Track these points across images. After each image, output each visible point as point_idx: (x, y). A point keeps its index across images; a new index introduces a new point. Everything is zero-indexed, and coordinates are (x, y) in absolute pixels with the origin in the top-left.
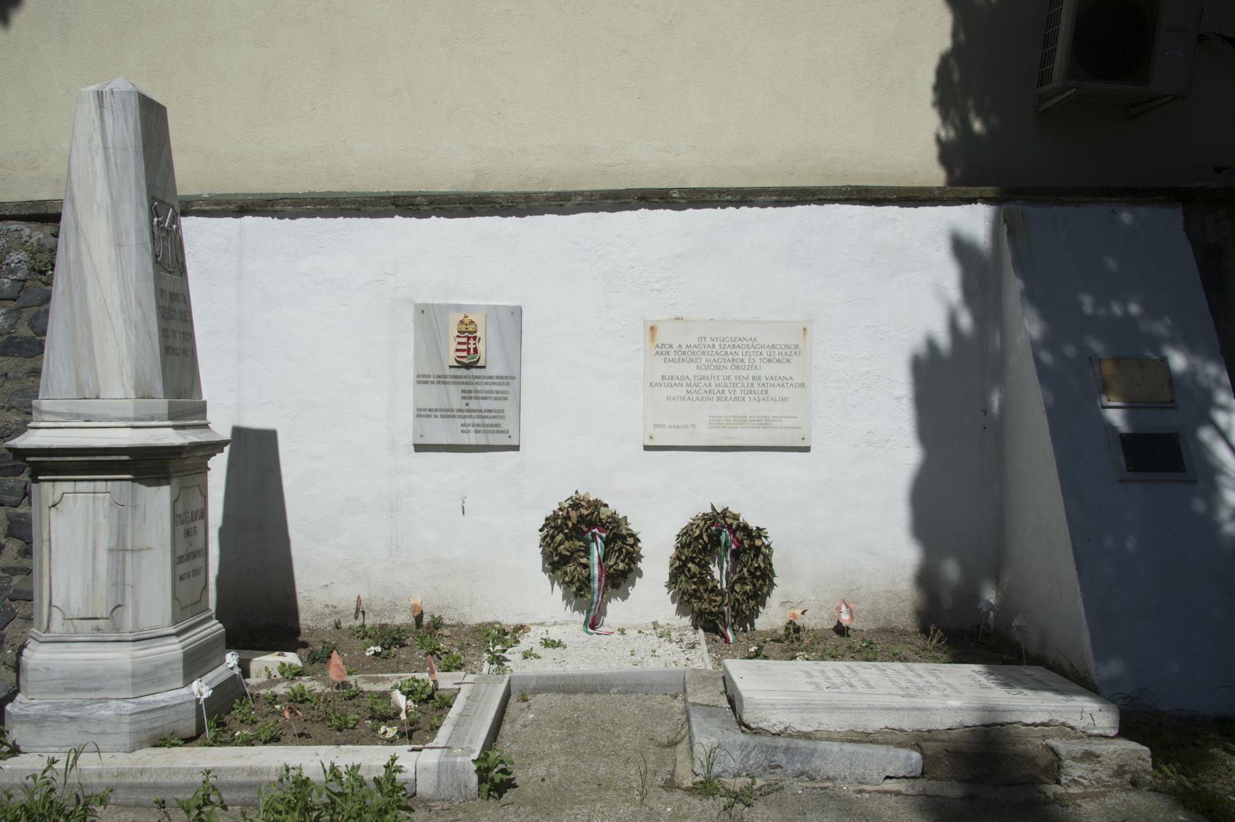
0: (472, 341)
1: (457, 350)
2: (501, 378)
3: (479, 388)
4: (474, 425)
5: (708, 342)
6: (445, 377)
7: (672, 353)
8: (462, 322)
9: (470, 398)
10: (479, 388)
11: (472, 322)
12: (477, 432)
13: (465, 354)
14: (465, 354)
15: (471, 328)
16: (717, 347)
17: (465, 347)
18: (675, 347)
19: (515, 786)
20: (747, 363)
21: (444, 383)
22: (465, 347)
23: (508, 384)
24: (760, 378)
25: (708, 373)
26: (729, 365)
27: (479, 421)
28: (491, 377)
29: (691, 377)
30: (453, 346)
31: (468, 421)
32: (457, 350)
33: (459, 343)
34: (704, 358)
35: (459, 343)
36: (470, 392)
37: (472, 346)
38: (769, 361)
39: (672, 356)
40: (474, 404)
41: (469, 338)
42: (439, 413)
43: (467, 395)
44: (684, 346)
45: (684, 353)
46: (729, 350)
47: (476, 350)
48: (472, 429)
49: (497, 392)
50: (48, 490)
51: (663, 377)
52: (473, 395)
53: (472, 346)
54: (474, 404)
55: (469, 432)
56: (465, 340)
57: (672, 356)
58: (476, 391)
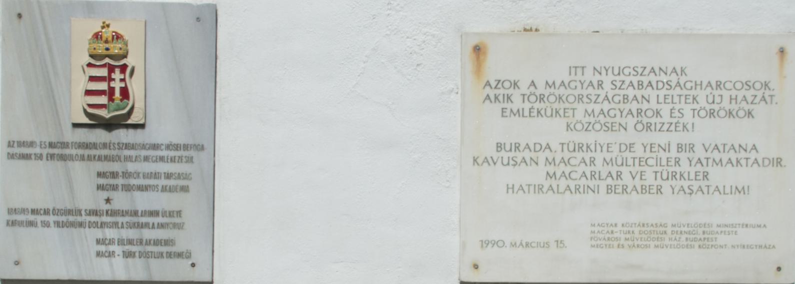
0: (117, 75)
1: (89, 93)
2: (177, 147)
3: (131, 167)
4: (121, 242)
5: (589, 76)
6: (65, 145)
8: (97, 36)
9: (114, 188)
10: (131, 167)
11: (118, 37)
12: (128, 255)
13: (103, 100)
14: (103, 100)
16: (607, 86)
17: (103, 86)
18: (524, 88)
20: (666, 118)
21: (63, 158)
22: (103, 86)
23: (190, 160)
24: (692, 148)
25: (588, 138)
26: (631, 121)
28: (155, 147)
29: (555, 146)
30: (81, 83)
31: (110, 233)
32: (89, 93)
33: (92, 79)
35: (92, 79)
36: (114, 175)
37: (117, 85)
38: (711, 114)
40: (121, 201)
41: (111, 69)
42: (51, 219)
43: (107, 182)
44: (541, 84)
45: (541, 98)
46: (631, 92)
47: (125, 93)
49: (168, 176)
51: (499, 147)
52: (120, 181)
53: (117, 85)
54: (121, 201)
55: (111, 254)
56: (104, 72)
58: (126, 175)
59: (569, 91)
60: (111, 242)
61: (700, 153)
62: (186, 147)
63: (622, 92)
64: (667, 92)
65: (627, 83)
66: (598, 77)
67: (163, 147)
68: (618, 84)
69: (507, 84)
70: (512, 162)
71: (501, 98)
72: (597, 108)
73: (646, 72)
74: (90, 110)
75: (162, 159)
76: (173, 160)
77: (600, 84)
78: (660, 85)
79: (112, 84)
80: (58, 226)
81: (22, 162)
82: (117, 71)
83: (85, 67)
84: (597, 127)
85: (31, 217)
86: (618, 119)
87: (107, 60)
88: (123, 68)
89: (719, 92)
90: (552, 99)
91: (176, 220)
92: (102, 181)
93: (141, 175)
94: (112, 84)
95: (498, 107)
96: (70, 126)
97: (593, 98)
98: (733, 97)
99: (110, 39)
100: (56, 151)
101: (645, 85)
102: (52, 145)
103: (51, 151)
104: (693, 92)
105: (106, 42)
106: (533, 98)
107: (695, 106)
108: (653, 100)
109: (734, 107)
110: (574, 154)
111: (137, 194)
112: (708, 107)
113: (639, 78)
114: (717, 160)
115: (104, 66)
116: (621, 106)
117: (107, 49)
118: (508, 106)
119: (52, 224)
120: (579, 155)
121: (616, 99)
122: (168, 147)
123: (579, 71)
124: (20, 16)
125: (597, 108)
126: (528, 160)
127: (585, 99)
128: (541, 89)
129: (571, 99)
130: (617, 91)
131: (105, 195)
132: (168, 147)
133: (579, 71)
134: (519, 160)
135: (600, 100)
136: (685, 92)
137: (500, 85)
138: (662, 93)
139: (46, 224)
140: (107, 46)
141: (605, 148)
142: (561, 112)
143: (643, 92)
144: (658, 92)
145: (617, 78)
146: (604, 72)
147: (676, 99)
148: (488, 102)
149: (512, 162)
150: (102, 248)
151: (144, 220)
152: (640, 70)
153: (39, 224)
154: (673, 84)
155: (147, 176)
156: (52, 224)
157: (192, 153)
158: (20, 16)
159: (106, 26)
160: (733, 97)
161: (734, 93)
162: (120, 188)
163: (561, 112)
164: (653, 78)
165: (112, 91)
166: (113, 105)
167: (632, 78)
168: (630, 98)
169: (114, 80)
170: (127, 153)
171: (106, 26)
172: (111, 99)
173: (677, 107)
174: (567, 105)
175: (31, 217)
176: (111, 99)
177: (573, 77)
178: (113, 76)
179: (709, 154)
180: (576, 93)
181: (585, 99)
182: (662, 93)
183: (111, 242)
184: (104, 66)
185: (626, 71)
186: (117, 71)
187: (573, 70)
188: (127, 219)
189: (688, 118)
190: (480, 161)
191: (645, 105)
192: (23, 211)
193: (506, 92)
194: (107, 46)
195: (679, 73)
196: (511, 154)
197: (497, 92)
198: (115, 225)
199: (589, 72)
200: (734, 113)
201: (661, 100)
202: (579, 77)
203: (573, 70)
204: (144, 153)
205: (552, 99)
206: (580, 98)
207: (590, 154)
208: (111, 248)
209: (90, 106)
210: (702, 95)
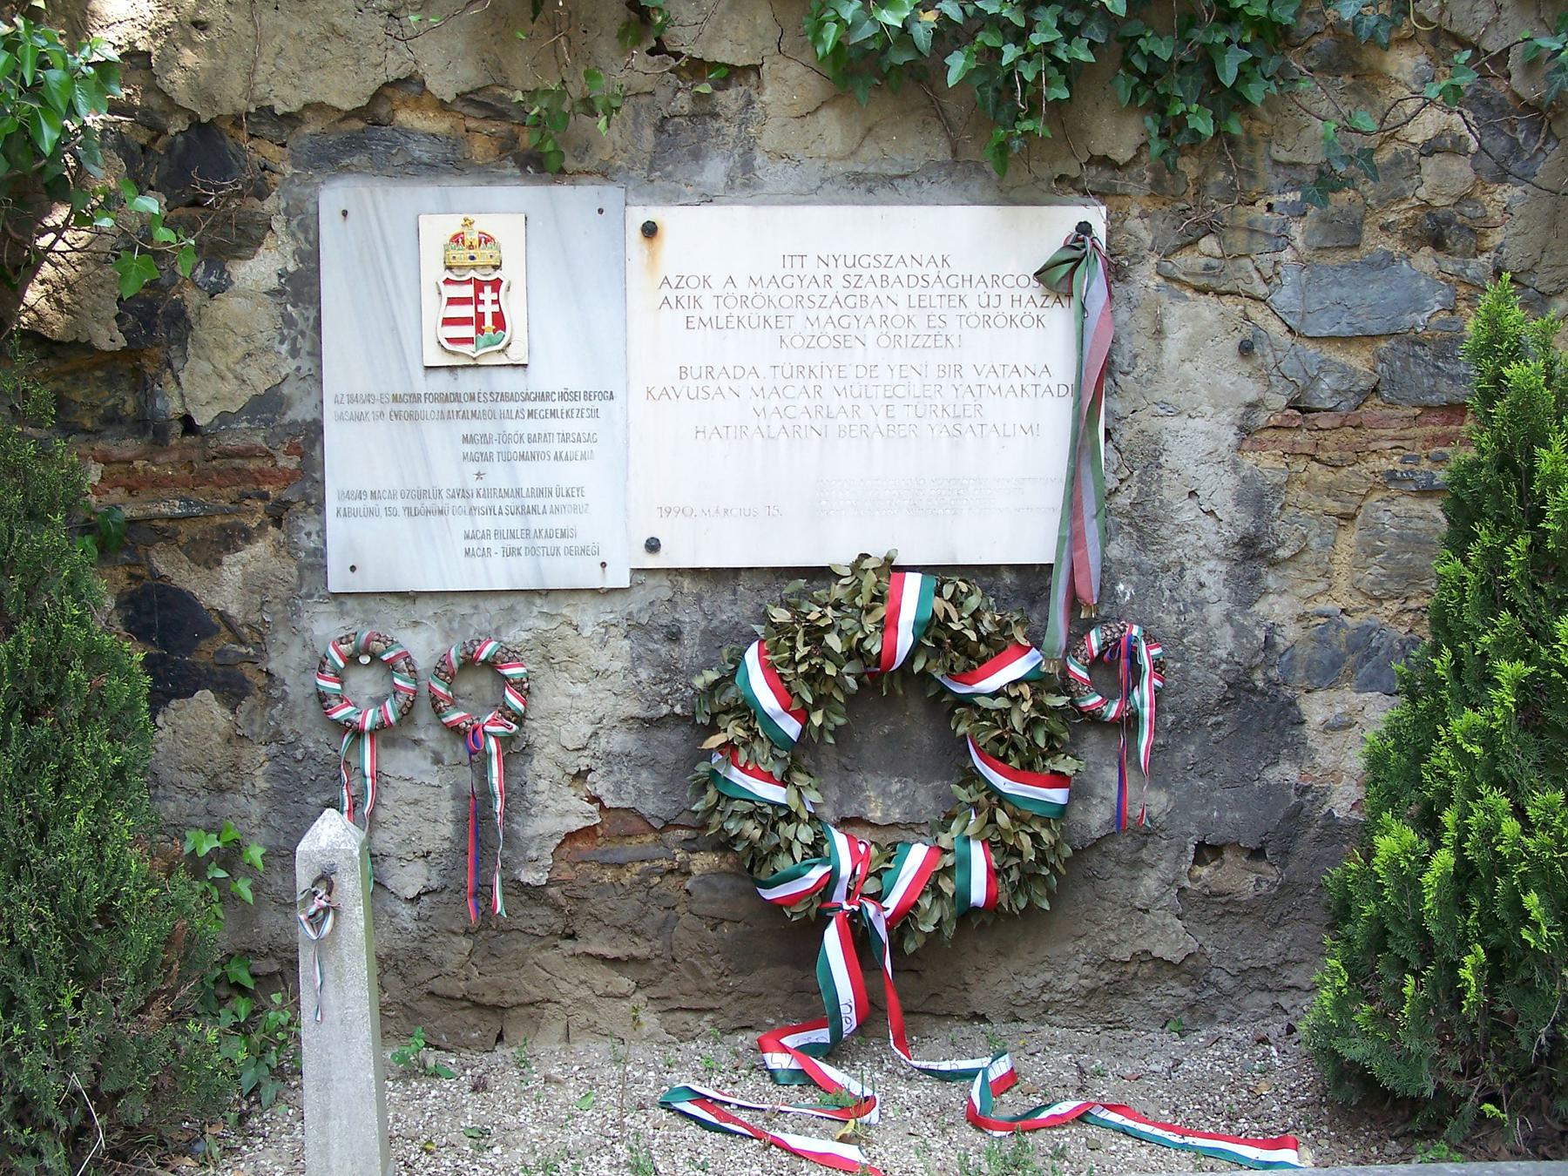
0: (487, 295)
1: (448, 322)
2: (575, 396)
3: (511, 426)
4: (498, 534)
5: (811, 268)
6: (415, 398)
7: (707, 298)
8: (457, 239)
9: (487, 458)
10: (511, 426)
11: (487, 240)
12: (511, 552)
13: (469, 331)
14: (469, 331)
15: (484, 255)
16: (837, 282)
17: (468, 311)
18: (717, 282)
19: (920, 977)
20: (922, 329)
21: (412, 416)
22: (468, 311)
23: (594, 413)
24: (958, 369)
25: (813, 358)
26: (871, 333)
27: (515, 522)
28: (543, 397)
29: (763, 370)
30: (434, 310)
31: (485, 523)
32: (448, 322)
33: (452, 301)
34: (799, 313)
35: (452, 301)
36: (485, 439)
37: (488, 309)
38: (987, 320)
39: (708, 309)
40: (498, 475)
41: (479, 286)
42: (399, 504)
43: (477, 450)
44: (743, 282)
45: (744, 300)
46: (871, 291)
47: (499, 321)
48: (494, 544)
49: (565, 438)
50: (908, 575)
51: (683, 372)
52: (494, 448)
53: (488, 309)
54: (498, 475)
55: (486, 553)
56: (468, 291)
57: (708, 309)
58: (505, 438)
59: (783, 291)
60: (485, 535)
61: (971, 377)
62: (588, 396)
63: (858, 292)
64: (924, 291)
65: (866, 278)
66: (823, 270)
67: (555, 397)
68: (853, 280)
69: (693, 282)
70: (702, 394)
71: (684, 302)
72: (824, 315)
73: (893, 262)
74: (448, 346)
75: (553, 414)
76: (569, 414)
77: (828, 279)
78: (913, 281)
79: (481, 309)
80: (410, 514)
81: (355, 425)
82: (488, 289)
83: (442, 285)
84: (824, 341)
85: (371, 503)
86: (853, 331)
87: (472, 274)
88: (496, 285)
89: (996, 290)
90: (758, 302)
91: (576, 501)
92: (468, 448)
93: (525, 438)
94: (481, 309)
95: (681, 314)
96: (421, 372)
97: (818, 301)
98: (1016, 297)
99: (476, 243)
100: (404, 407)
101: (891, 281)
102: (396, 399)
103: (396, 407)
104: (957, 292)
105: (471, 247)
106: (731, 302)
107: (962, 310)
108: (903, 303)
109: (1018, 311)
110: (791, 382)
111: (521, 466)
112: (981, 312)
113: (882, 271)
114: (995, 388)
115: (468, 282)
116: (858, 312)
117: (472, 258)
118: (697, 313)
119: (401, 512)
120: (799, 382)
121: (850, 302)
122: (562, 396)
123: (797, 261)
124: (345, 213)
125: (824, 315)
126: (725, 391)
127: (806, 303)
128: (744, 288)
129: (786, 302)
130: (851, 291)
131: (473, 468)
132: (562, 396)
133: (797, 261)
134: (711, 391)
135: (827, 302)
136: (948, 291)
137: (683, 283)
138: (915, 292)
139: (391, 512)
140: (472, 252)
141: (835, 372)
142: (772, 321)
143: (888, 291)
144: (911, 291)
145: (852, 272)
146: (832, 262)
147: (936, 301)
148: (666, 306)
149: (702, 394)
150: (473, 544)
151: (530, 502)
152: (884, 260)
153: (383, 512)
154: (931, 280)
155: (532, 439)
156: (401, 512)
157: (596, 404)
158: (345, 213)
159: (468, 223)
160: (1016, 297)
161: (1017, 292)
162: (495, 457)
163: (772, 321)
164: (903, 271)
165: (480, 317)
166: (482, 339)
167: (871, 271)
168: (871, 299)
169: (483, 302)
170: (505, 406)
171: (468, 223)
172: (480, 331)
173: (938, 312)
174: (780, 312)
175: (371, 503)
176: (480, 331)
177: (788, 270)
178: (481, 297)
179: (982, 380)
180: (793, 292)
181: (806, 303)
182: (915, 292)
183: (485, 535)
184: (468, 282)
185: (864, 261)
186: (488, 289)
187: (788, 260)
188: (508, 501)
189: (953, 328)
190: (656, 393)
191: (891, 311)
192: (360, 495)
193: (692, 293)
194: (472, 252)
195: (939, 263)
196: (701, 383)
197: (679, 293)
198: (491, 511)
199: (811, 262)
200: (1017, 320)
201: (915, 302)
202: (797, 270)
203: (788, 260)
204: (529, 406)
205: (758, 302)
206: (799, 300)
207: (813, 381)
208: (486, 544)
209: (449, 340)
210: (972, 295)
